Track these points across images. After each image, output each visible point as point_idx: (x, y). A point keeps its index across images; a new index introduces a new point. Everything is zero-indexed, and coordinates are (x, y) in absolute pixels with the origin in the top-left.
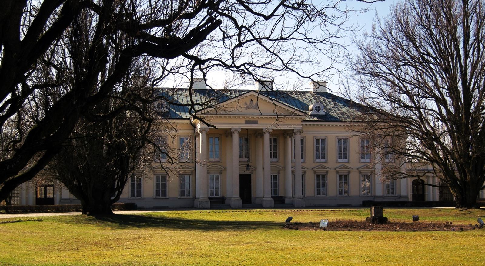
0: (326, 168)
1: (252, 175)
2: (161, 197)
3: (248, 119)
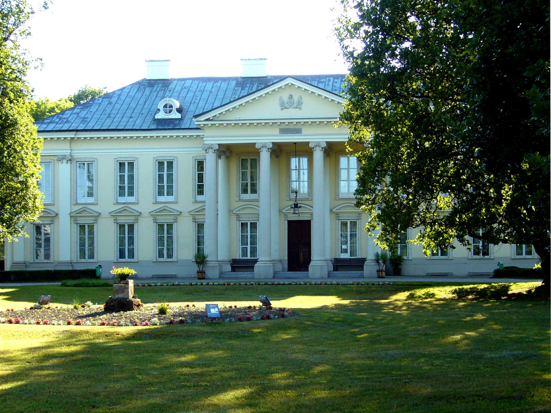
0: (171, 212)
3: (283, 127)
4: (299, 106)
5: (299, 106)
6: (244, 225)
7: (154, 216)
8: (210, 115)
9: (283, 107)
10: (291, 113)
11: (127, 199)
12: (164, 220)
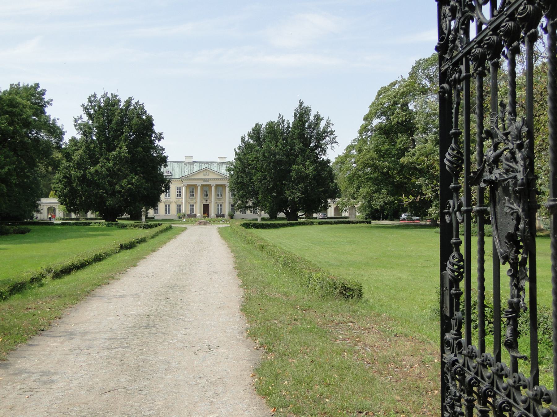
4: (208, 175)
5: (208, 175)
6: (191, 205)
10: (206, 177)
12: (167, 204)
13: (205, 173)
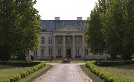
1: (71, 49)
2: (94, 55)
7: (48, 48)
8: (55, 31)
9: (67, 29)
10: (69, 30)
11: (43, 44)
13: (68, 27)
